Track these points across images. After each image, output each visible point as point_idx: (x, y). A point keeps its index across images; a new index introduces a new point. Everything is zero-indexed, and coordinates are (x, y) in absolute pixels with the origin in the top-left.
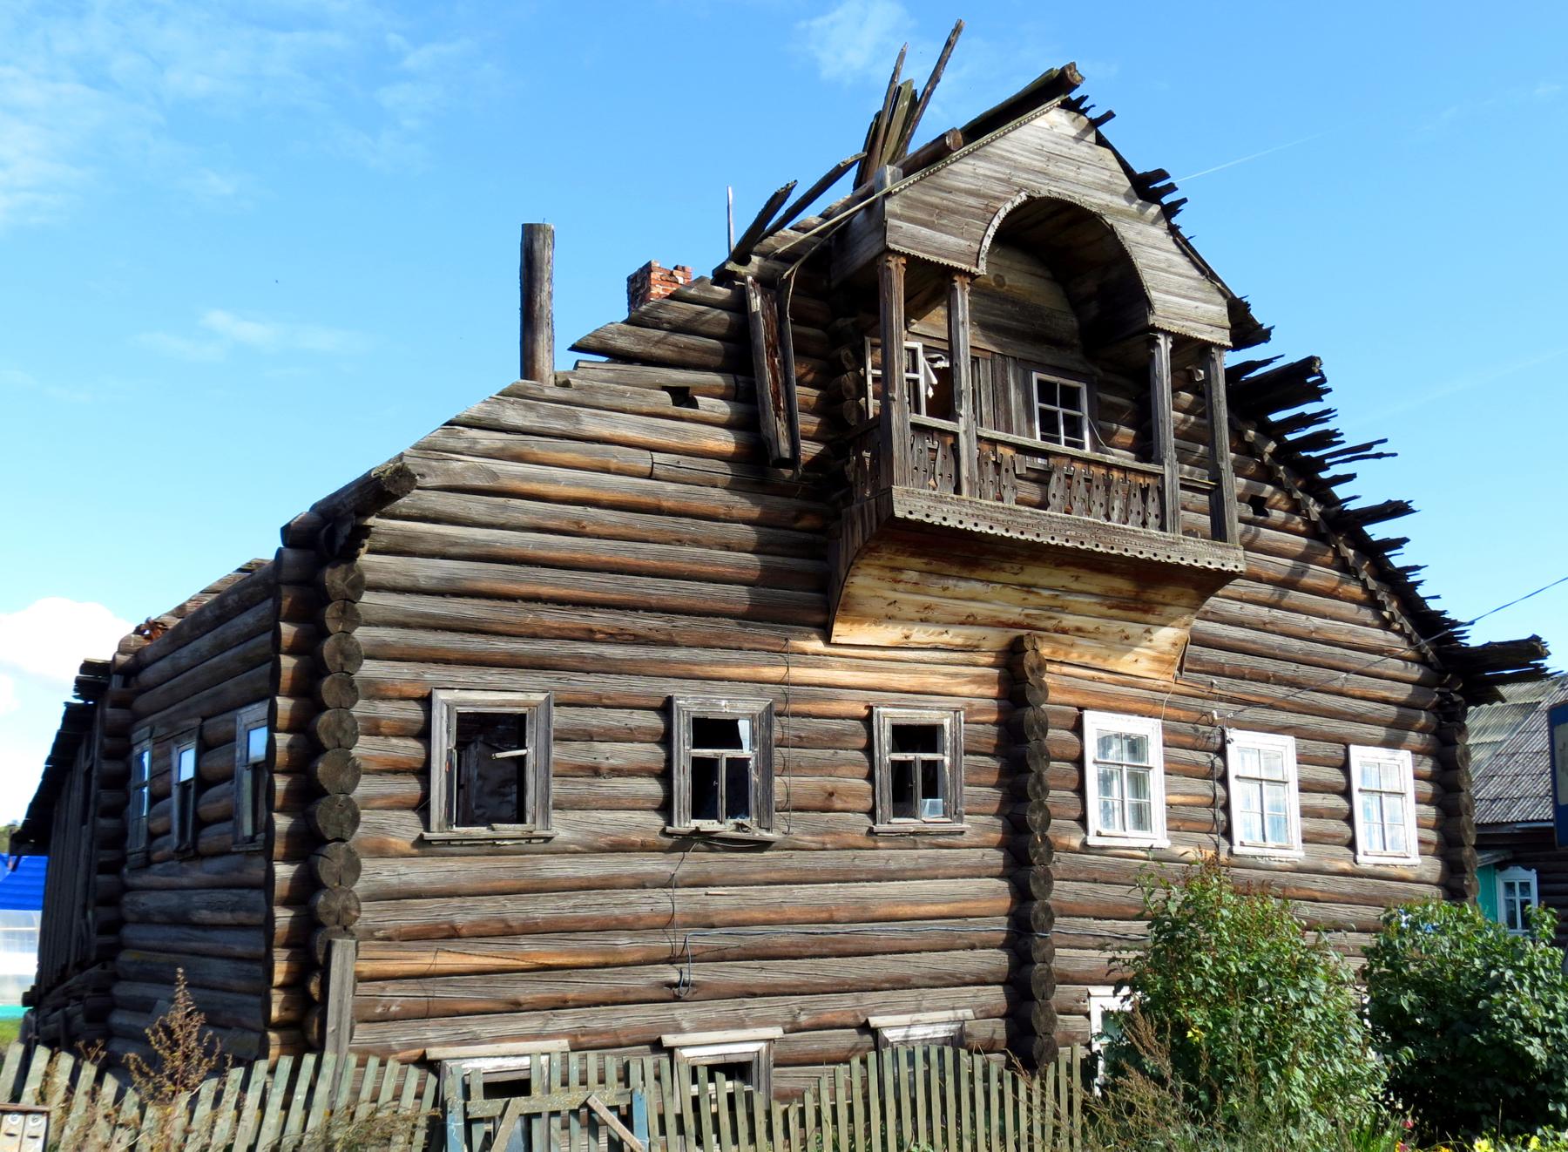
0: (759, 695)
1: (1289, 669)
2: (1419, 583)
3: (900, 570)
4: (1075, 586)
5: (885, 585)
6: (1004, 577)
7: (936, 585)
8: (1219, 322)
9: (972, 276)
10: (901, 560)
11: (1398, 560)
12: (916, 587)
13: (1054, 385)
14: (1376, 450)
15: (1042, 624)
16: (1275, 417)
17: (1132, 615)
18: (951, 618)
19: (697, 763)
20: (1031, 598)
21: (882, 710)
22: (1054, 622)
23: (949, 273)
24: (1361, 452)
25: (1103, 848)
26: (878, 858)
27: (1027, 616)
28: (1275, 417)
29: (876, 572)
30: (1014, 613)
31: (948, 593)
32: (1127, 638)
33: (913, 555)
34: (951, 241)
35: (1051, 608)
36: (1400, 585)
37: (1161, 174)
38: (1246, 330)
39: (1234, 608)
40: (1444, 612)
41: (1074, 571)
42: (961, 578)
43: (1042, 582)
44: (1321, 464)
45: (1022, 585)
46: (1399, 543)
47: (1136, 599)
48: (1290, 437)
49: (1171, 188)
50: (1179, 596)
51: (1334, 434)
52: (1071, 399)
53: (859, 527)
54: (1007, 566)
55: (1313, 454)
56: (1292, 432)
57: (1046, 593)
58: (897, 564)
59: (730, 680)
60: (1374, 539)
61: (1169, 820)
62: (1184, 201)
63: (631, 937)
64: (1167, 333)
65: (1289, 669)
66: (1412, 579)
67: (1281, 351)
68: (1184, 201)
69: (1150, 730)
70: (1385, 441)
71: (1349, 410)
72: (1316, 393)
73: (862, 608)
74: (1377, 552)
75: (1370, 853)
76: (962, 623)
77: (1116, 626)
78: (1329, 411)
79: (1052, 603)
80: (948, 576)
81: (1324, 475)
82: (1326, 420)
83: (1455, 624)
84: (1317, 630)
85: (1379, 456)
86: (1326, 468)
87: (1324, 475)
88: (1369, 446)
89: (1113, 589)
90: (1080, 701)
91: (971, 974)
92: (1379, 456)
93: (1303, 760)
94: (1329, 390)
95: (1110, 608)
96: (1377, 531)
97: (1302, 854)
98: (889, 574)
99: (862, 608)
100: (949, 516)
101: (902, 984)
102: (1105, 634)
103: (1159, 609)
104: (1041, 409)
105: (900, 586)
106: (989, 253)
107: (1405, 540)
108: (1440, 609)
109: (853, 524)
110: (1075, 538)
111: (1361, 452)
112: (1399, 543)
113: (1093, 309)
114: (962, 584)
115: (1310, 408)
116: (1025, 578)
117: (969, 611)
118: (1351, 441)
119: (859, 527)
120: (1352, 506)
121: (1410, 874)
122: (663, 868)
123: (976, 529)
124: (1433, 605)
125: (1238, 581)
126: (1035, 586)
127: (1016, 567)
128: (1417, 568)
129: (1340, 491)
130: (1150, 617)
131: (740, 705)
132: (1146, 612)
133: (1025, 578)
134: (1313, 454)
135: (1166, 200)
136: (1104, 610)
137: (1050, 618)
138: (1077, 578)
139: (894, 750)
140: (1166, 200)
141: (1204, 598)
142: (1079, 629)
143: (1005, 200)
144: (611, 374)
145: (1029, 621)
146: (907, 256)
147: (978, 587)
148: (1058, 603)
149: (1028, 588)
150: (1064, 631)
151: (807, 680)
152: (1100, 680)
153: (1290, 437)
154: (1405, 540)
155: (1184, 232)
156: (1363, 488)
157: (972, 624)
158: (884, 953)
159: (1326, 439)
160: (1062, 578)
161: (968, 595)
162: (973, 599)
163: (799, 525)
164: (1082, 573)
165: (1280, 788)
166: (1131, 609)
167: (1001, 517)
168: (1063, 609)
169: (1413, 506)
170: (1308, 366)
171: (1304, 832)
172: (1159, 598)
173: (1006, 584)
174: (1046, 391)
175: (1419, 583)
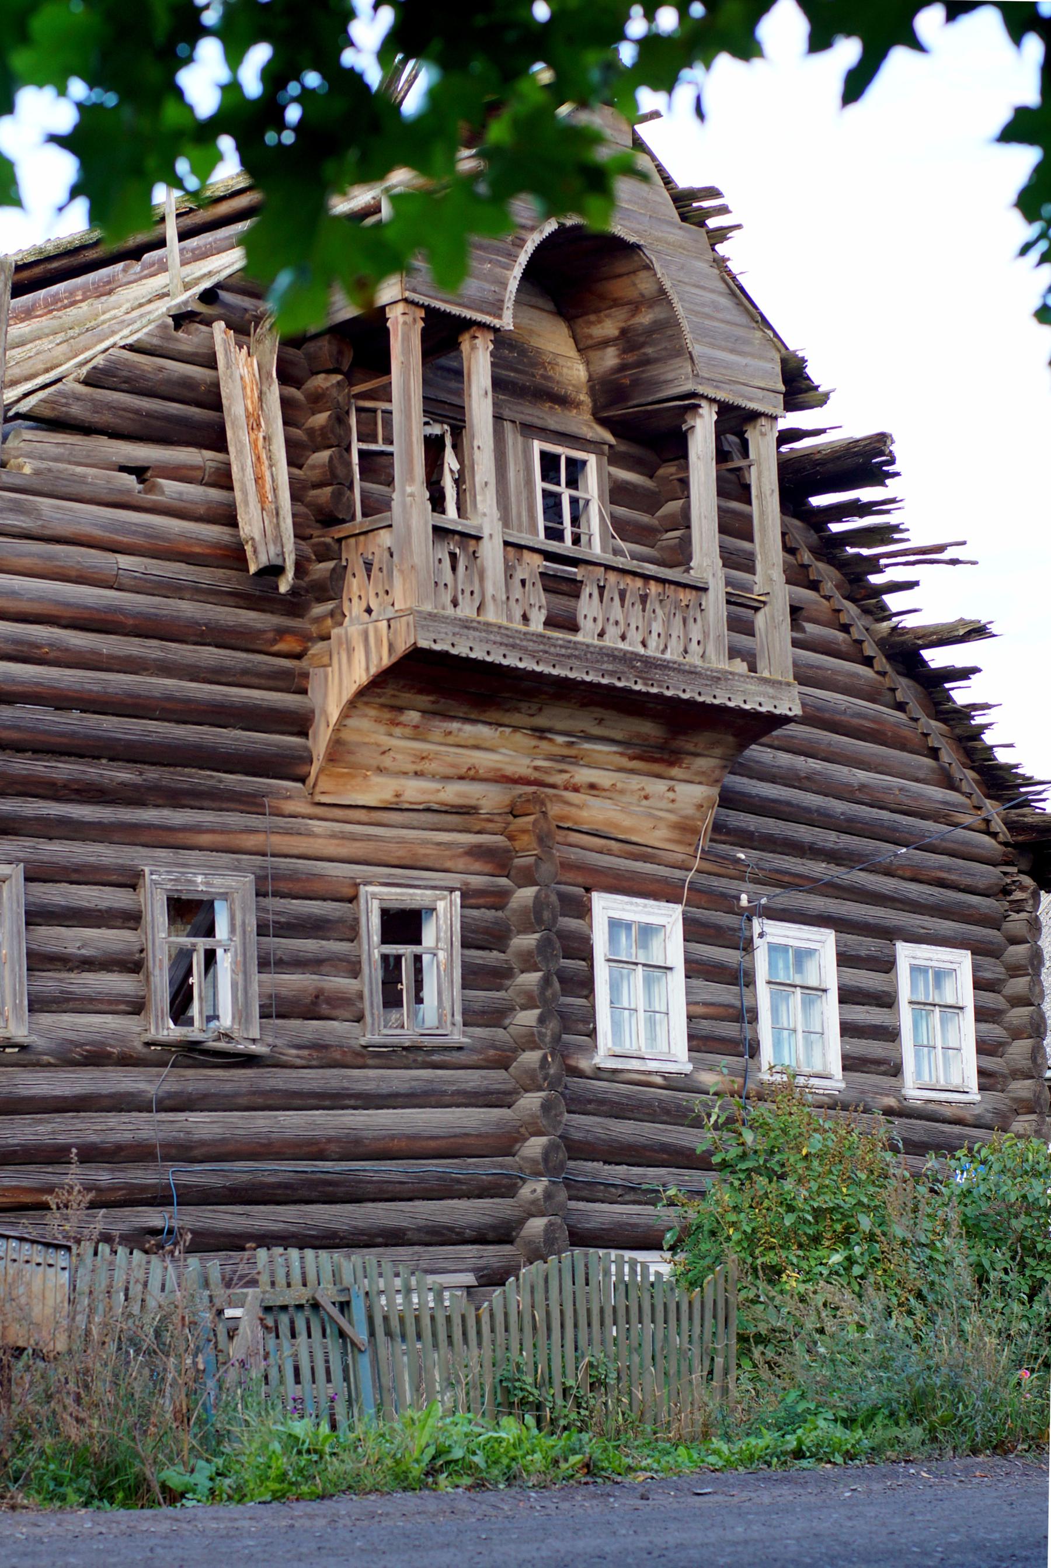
0: (236, 869)
1: (831, 839)
2: (986, 726)
3: (401, 709)
4: (597, 731)
5: (382, 729)
6: (517, 719)
7: (440, 727)
8: (771, 385)
9: (496, 330)
10: (407, 697)
11: (961, 695)
12: (418, 733)
13: (557, 457)
14: (946, 555)
15: (551, 780)
16: (819, 501)
17: (656, 768)
18: (450, 771)
19: (385, 958)
20: (544, 745)
21: (370, 889)
22: (566, 776)
24: (929, 554)
25: (615, 1071)
26: (368, 1079)
27: (536, 768)
28: (819, 501)
29: (373, 713)
30: (521, 765)
31: (450, 740)
32: (646, 798)
33: (421, 692)
35: (563, 759)
36: (964, 730)
37: (713, 193)
38: (797, 387)
39: (785, 759)
40: (1016, 766)
41: (599, 712)
42: (467, 720)
43: (559, 726)
44: (874, 565)
45: (534, 729)
46: (965, 674)
47: (661, 748)
48: (835, 527)
49: (724, 210)
50: (713, 744)
51: (896, 528)
52: (576, 467)
53: (359, 655)
54: (524, 706)
55: (865, 552)
56: (840, 521)
57: (560, 739)
58: (398, 703)
59: (201, 849)
60: (933, 665)
61: (691, 1037)
62: (738, 227)
63: (112, 1170)
64: (712, 401)
65: (831, 839)
66: (978, 721)
67: (837, 422)
68: (738, 227)
69: (669, 917)
70: (964, 543)
71: (916, 501)
72: (878, 476)
73: (352, 758)
74: (935, 683)
75: (916, 1083)
76: (461, 778)
77: (635, 782)
78: (893, 501)
79: (566, 752)
80: (453, 718)
81: (875, 579)
82: (888, 512)
83: (1029, 781)
84: (863, 787)
85: (954, 562)
86: (880, 570)
87: (875, 579)
88: (941, 548)
89: (638, 735)
90: (590, 881)
91: (470, 1228)
92: (954, 562)
93: (844, 960)
94: (897, 474)
95: (632, 758)
96: (937, 658)
97: (842, 1085)
98: (387, 715)
99: (352, 758)
100: (476, 648)
101: (393, 1238)
102: (622, 792)
103: (688, 760)
104: (544, 491)
105: (398, 731)
106: (517, 301)
107: (975, 670)
108: (1012, 761)
109: (350, 651)
110: (612, 674)
111: (929, 554)
112: (965, 674)
113: (610, 358)
114: (468, 728)
115: (867, 494)
116: (541, 721)
117: (470, 761)
118: (917, 539)
119: (359, 655)
120: (909, 622)
121: (967, 1115)
122: (142, 1086)
123: (489, 659)
124: (1003, 756)
125: (792, 726)
126: (550, 730)
127: (535, 707)
128: (987, 706)
129: (893, 601)
130: (675, 771)
131: (217, 881)
132: (671, 764)
133: (541, 721)
134: (865, 552)
135: (712, 223)
136: (625, 762)
137: (562, 771)
138: (600, 721)
139: (385, 941)
140: (712, 223)
141: (743, 746)
142: (592, 786)
143: (533, 229)
144: (61, 450)
145: (536, 775)
146: (428, 309)
147: (484, 732)
148: (572, 752)
149: (540, 733)
150: (576, 789)
151: (286, 850)
152: (610, 853)
153: (835, 527)
154: (975, 670)
155: (733, 266)
156: (924, 601)
157: (473, 779)
158: (373, 1200)
159: (884, 534)
160: (584, 722)
161: (471, 742)
162: (477, 747)
163: (276, 648)
164: (606, 714)
165: (914, 999)
166: (655, 760)
167: (531, 646)
168: (575, 760)
169: (993, 628)
170: (879, 443)
171: (845, 1057)
172: (690, 747)
173: (516, 728)
174: (549, 462)
175: (986, 726)
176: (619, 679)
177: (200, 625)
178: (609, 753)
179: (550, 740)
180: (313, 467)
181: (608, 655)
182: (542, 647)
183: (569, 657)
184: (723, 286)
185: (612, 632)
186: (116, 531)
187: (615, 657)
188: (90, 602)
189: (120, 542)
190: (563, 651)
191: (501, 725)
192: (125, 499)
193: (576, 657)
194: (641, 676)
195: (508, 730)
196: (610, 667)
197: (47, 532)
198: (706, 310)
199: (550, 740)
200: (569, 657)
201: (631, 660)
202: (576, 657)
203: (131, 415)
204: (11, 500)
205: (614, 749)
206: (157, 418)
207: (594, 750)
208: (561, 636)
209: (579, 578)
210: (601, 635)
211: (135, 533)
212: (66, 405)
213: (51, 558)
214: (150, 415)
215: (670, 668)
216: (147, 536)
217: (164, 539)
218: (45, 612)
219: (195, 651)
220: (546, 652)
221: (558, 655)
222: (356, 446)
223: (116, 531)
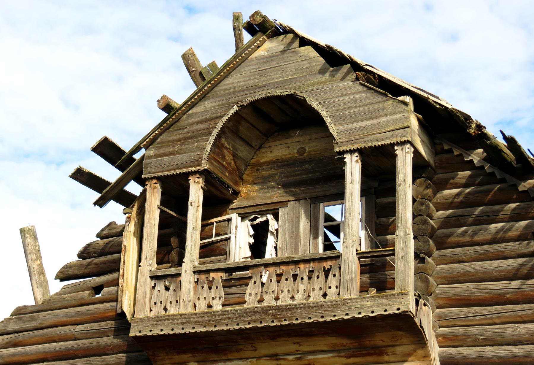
23: (187, 175)
34: (182, 158)
95: (348, 357)
110: (255, 321)
176: (261, 323)
177: (110, 346)
178: (329, 358)
179: (284, 359)
180: (507, 210)
181: (250, 312)
182: (207, 319)
183: (224, 319)
184: (361, 87)
185: (267, 297)
186: (72, 317)
187: (255, 312)
188: (58, 349)
189: (75, 321)
190: (221, 317)
191: (248, 359)
192: (83, 301)
193: (229, 318)
194: (274, 317)
195: (254, 360)
196: (254, 318)
197: (44, 325)
198: (349, 105)
199: (284, 359)
200: (224, 319)
201: (267, 311)
202: (229, 318)
203: (94, 266)
204: (30, 317)
205: (330, 355)
206: (105, 263)
207: (317, 358)
208: (238, 308)
209: (250, 275)
210: (325, 295)
211: (80, 315)
212: (67, 271)
213: (45, 335)
214: (102, 263)
215: (297, 308)
216: (86, 315)
217: (94, 314)
218: (39, 357)
219: (111, 357)
220: (210, 320)
221: (217, 320)
222: (214, 239)
223: (72, 317)
